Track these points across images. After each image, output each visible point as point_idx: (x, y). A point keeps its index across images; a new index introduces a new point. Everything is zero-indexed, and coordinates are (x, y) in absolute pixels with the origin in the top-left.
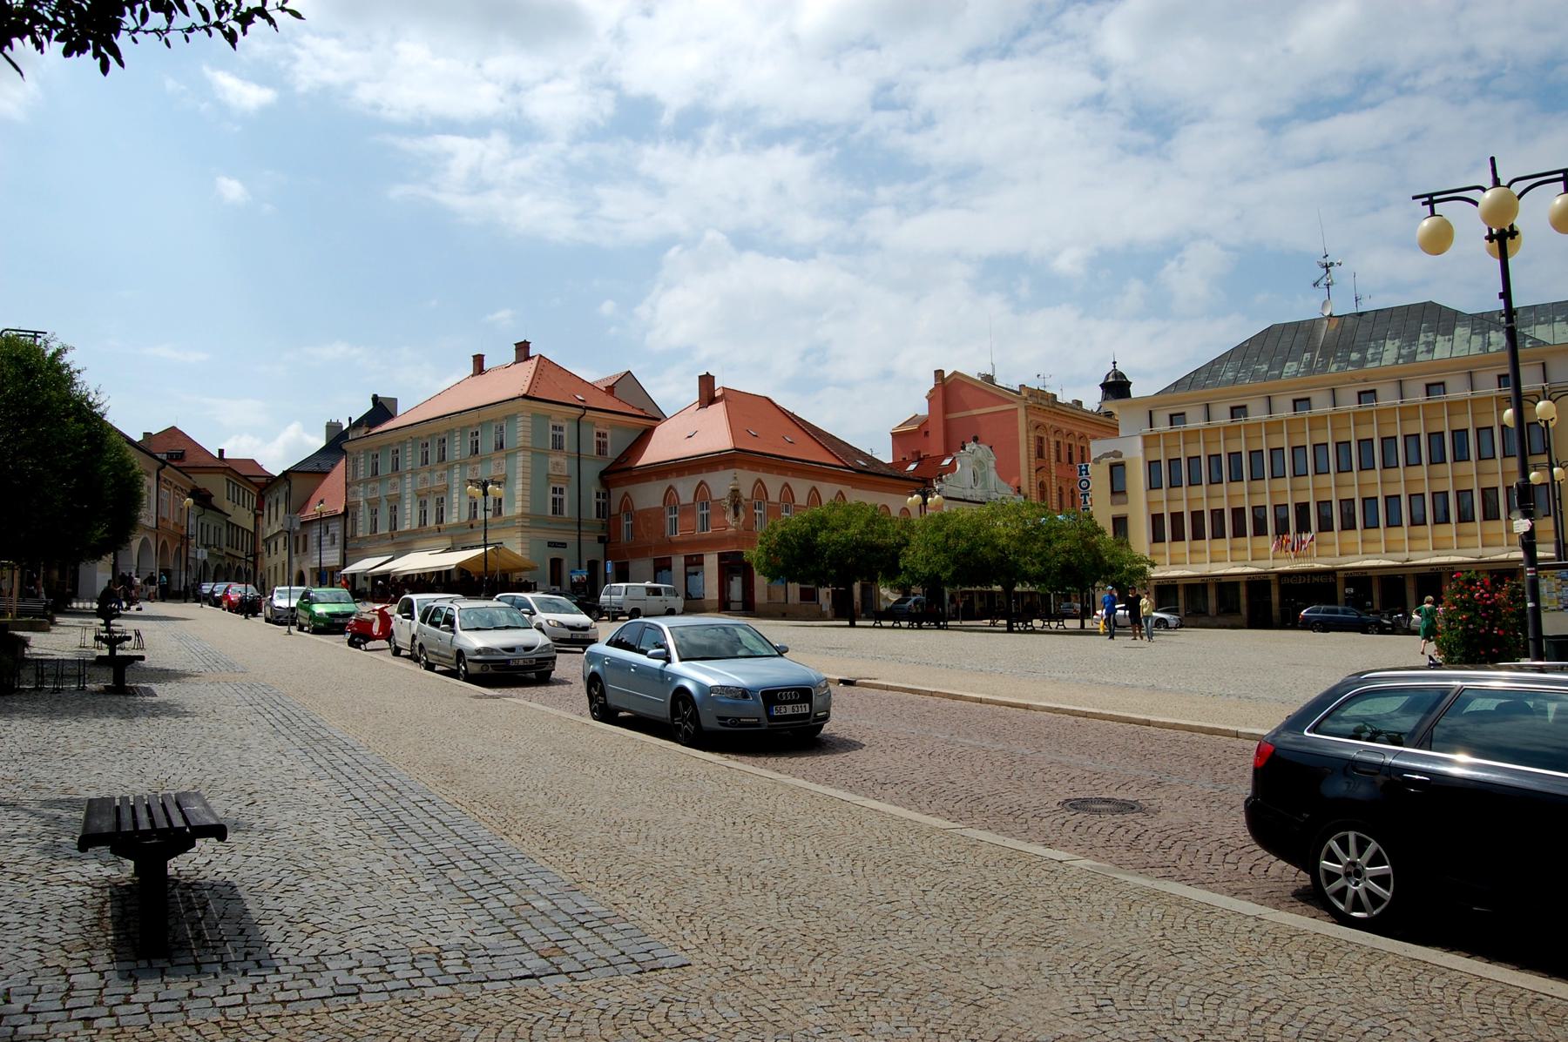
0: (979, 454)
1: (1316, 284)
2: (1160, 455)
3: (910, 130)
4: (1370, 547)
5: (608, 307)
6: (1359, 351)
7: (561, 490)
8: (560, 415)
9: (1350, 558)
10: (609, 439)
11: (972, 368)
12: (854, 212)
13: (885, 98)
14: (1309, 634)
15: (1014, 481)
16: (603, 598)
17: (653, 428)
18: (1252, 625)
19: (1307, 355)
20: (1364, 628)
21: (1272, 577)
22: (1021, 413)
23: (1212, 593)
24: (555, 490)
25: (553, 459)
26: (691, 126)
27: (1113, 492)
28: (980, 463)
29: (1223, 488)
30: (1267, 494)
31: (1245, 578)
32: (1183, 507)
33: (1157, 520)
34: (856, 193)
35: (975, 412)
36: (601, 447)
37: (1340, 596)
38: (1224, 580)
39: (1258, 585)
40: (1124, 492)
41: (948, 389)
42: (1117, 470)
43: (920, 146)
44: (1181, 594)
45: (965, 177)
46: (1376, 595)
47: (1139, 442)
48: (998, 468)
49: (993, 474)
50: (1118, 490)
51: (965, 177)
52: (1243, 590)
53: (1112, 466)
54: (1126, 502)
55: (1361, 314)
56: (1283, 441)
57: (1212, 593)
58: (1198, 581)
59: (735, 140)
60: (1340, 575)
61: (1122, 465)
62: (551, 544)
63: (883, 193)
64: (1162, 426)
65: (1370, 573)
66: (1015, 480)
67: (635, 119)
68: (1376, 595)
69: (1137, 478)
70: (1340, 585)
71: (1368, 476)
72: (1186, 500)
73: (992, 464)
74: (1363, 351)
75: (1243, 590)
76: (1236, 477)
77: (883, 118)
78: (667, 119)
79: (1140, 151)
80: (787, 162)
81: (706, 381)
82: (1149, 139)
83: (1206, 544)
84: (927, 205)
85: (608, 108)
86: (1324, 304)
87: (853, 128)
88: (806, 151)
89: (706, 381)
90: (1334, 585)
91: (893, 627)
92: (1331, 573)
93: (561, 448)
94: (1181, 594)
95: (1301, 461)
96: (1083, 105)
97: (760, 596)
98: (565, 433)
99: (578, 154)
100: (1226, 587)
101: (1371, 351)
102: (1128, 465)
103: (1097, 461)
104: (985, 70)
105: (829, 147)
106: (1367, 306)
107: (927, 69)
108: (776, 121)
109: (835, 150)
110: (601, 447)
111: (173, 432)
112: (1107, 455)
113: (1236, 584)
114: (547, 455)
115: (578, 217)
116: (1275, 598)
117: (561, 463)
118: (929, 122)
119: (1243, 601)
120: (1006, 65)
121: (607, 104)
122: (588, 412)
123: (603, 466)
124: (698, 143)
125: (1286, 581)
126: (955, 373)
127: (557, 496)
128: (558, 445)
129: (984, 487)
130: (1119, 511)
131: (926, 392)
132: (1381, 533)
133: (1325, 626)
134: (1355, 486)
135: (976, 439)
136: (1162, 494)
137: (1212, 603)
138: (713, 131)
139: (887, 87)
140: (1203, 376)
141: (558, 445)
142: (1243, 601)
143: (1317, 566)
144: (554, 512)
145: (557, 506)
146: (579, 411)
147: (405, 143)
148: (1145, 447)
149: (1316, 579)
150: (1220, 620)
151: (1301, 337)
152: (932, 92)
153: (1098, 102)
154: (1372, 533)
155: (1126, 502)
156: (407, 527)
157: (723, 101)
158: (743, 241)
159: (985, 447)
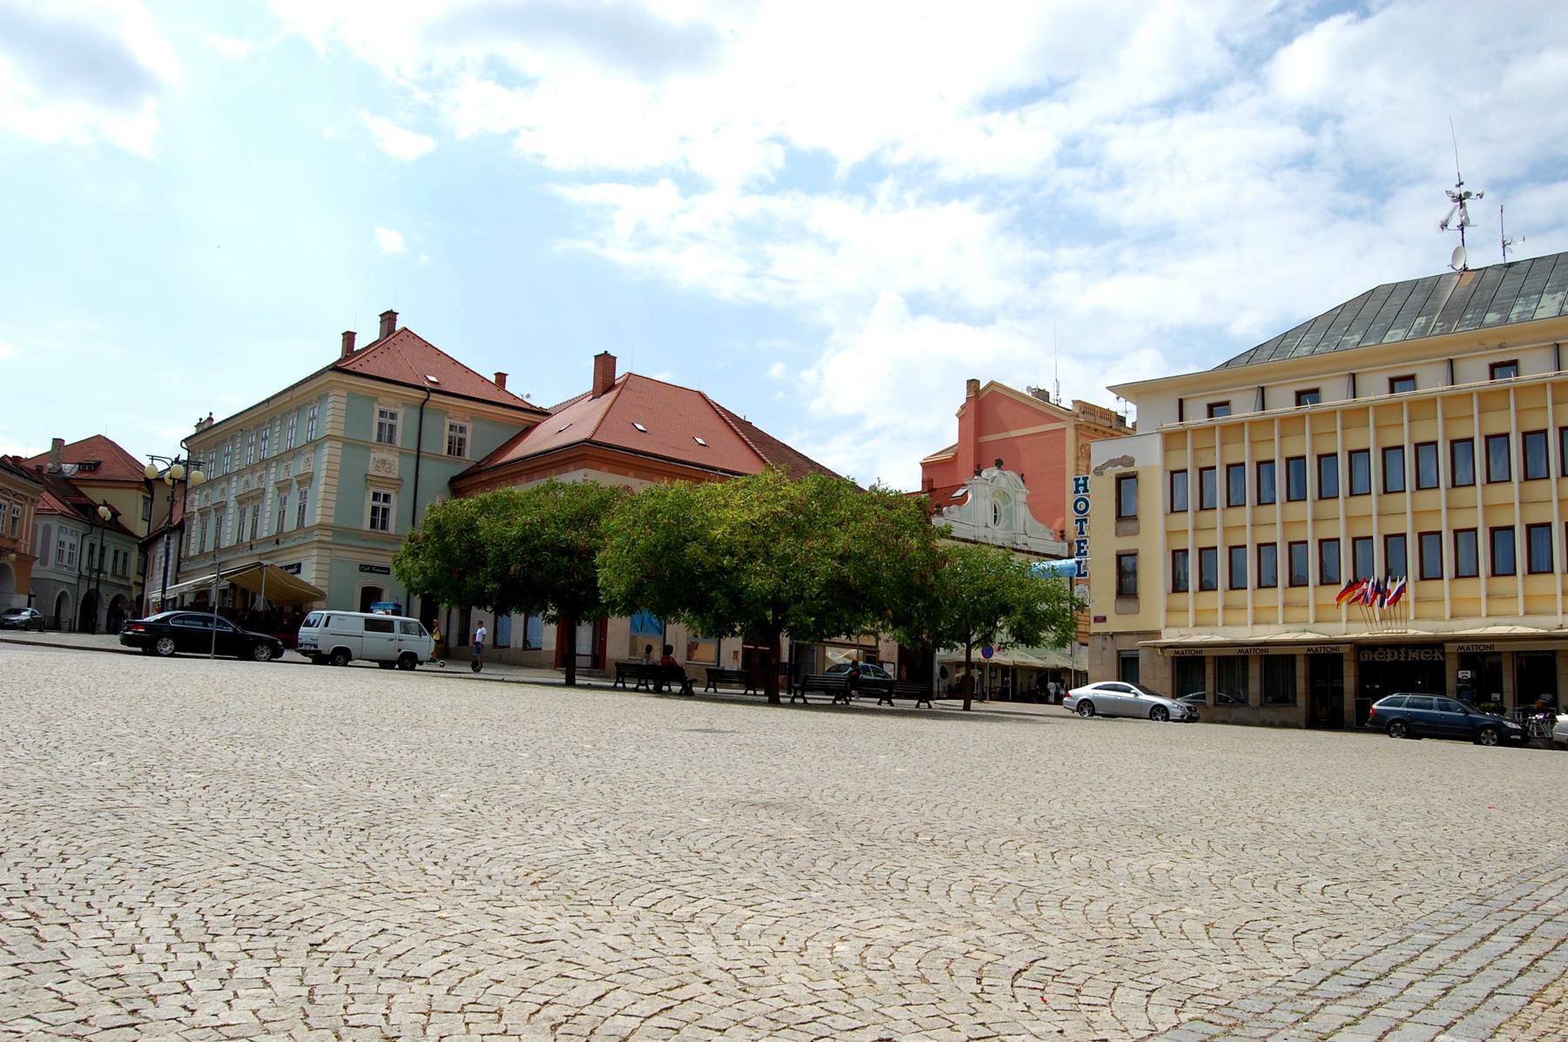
0: (1003, 482)
1: (1444, 225)
2: (1185, 459)
3: (1097, 189)
4: (1499, 606)
5: (777, 370)
6: (1499, 311)
7: (387, 498)
8: (391, 399)
9: (1468, 622)
10: (468, 436)
11: (1019, 382)
12: (1037, 275)
13: (1072, 153)
14: (1382, 740)
15: (1057, 525)
16: (304, 631)
17: (537, 424)
18: (1313, 723)
19: (1422, 320)
20: (1473, 734)
21: (1344, 649)
22: (1070, 434)
23: (1254, 671)
24: (376, 496)
25: (377, 455)
26: (864, 179)
27: (1119, 517)
28: (1005, 495)
29: (1276, 512)
30: (1341, 518)
31: (1303, 650)
32: (1216, 539)
33: (1178, 556)
34: (1039, 255)
35: (1014, 433)
36: (456, 447)
37: (1451, 684)
38: (1272, 651)
39: (1324, 660)
40: (1134, 518)
41: (984, 406)
42: (1126, 482)
43: (1107, 205)
44: (1209, 671)
45: (1161, 238)
46: (1508, 683)
47: (1157, 442)
48: (1032, 505)
49: (1023, 512)
50: (1125, 517)
51: (1161, 238)
52: (1301, 669)
53: (1119, 480)
54: (1136, 533)
55: (1510, 265)
56: (1368, 438)
57: (1254, 671)
58: (1233, 652)
59: (909, 197)
60: (1450, 648)
61: (1133, 476)
62: (363, 568)
63: (1065, 254)
64: (1197, 417)
65: (1498, 647)
66: (1059, 521)
67: (806, 172)
68: (1508, 683)
69: (1152, 497)
70: (1451, 665)
71: (1499, 493)
72: (1221, 528)
73: (1022, 497)
74: (1505, 310)
75: (1301, 669)
76: (1296, 494)
77: (1069, 175)
78: (841, 172)
79: (1355, 214)
80: (966, 219)
81: (605, 363)
82: (1366, 202)
83: (1247, 596)
84: (1114, 269)
85: (779, 161)
86: (1456, 254)
87: (1036, 186)
88: (985, 208)
89: (605, 363)
90: (1441, 666)
91: (615, 688)
92: (1435, 645)
93: (391, 440)
94: (1209, 671)
95: (1395, 468)
96: (1289, 166)
97: (618, 647)
98: (399, 423)
99: (751, 207)
100: (1275, 663)
101: (1517, 309)
102: (1140, 477)
103: (1099, 472)
104: (1184, 123)
105: (1008, 206)
106: (1521, 252)
107: (1118, 122)
108: (952, 174)
109: (1016, 208)
110: (456, 447)
111: (100, 441)
112: (1113, 463)
113: (1291, 659)
114: (367, 447)
115: (751, 275)
116: (1349, 682)
117: (390, 463)
118: (1117, 181)
119: (1301, 685)
120: (1204, 118)
121: (778, 158)
122: (434, 397)
123: (457, 470)
124: (871, 199)
125: (1367, 656)
126: (992, 383)
127: (380, 504)
128: (387, 435)
129: (1009, 527)
130: (1126, 544)
131: (957, 409)
132: (1518, 583)
133: (1412, 728)
134: (1478, 507)
135: (999, 464)
136: (1187, 521)
137: (1255, 686)
138: (885, 189)
139: (1072, 143)
140: (1266, 354)
141: (387, 435)
142: (1301, 685)
143: (1411, 632)
144: (373, 525)
145: (379, 517)
146: (422, 395)
147: (558, 190)
148: (1166, 449)
149: (1413, 655)
150: (1221, 712)
151: (1417, 298)
152: (1124, 147)
153: (1306, 162)
154: (1503, 583)
155: (1136, 533)
156: (227, 544)
157: (900, 157)
158: (918, 305)
159: (1010, 474)
